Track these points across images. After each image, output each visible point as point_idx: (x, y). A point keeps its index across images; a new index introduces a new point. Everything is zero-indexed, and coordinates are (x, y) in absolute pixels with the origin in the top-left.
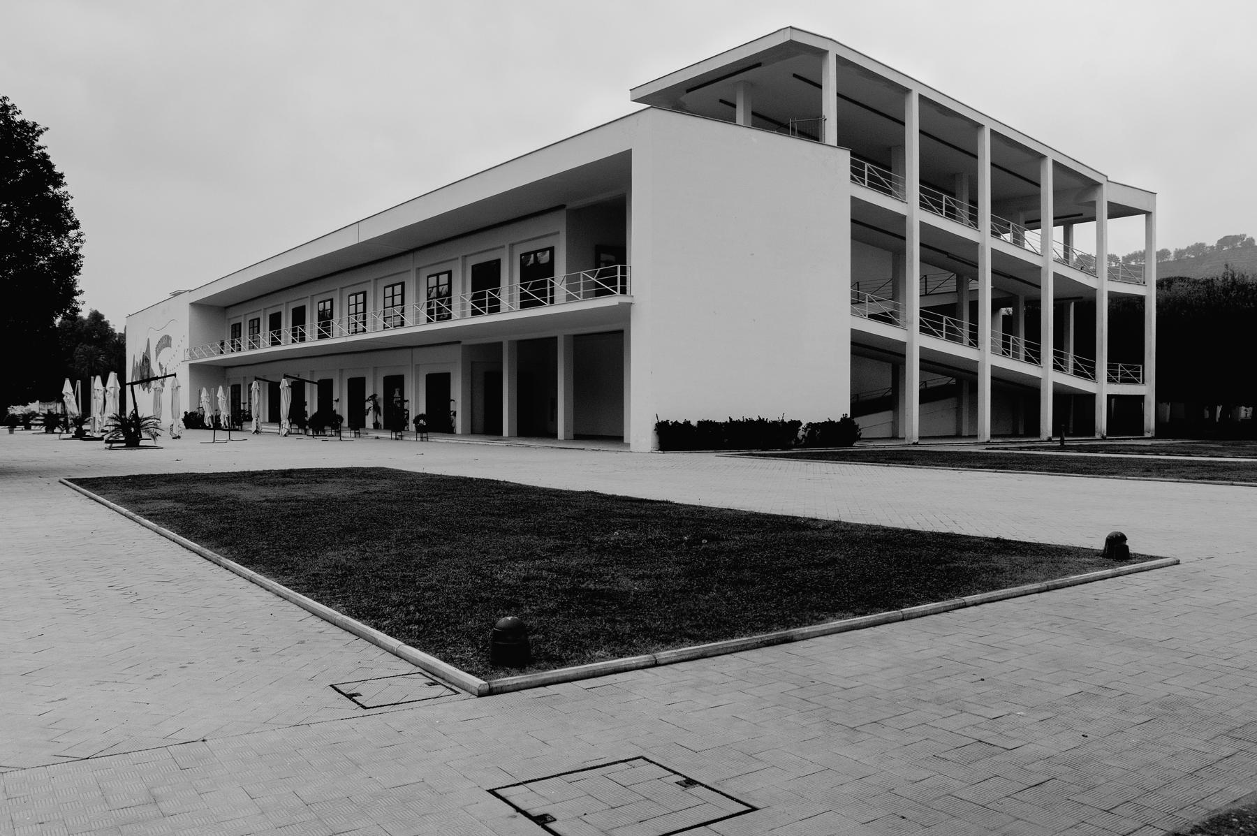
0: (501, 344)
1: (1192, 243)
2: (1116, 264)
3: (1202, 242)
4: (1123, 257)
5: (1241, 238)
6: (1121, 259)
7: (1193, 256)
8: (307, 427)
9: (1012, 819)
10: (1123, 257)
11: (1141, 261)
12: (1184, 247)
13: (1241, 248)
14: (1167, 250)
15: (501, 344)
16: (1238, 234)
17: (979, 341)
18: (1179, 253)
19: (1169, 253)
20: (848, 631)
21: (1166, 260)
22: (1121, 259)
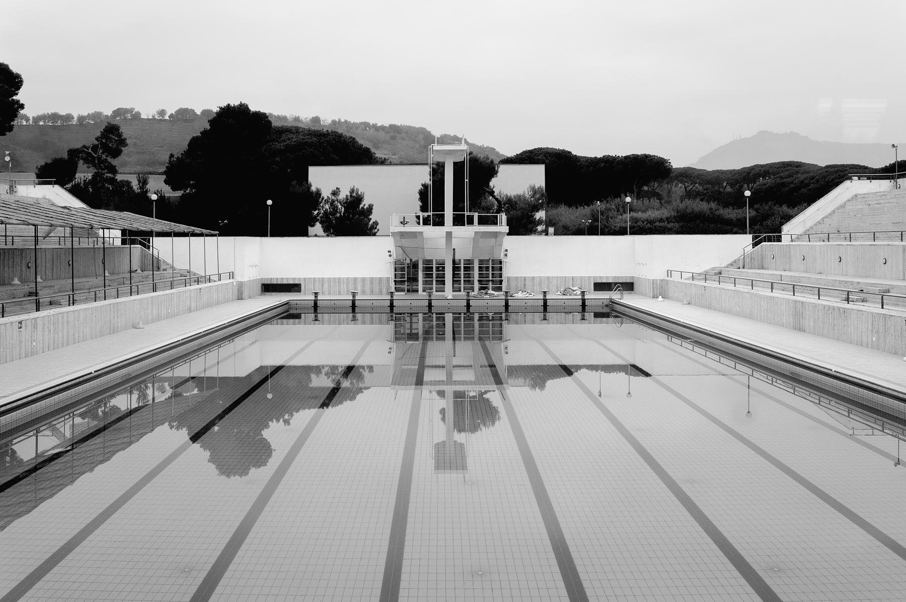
0: (479, 223)
1: (91, 111)
2: (27, 122)
3: (101, 111)
4: (33, 117)
5: (130, 111)
6: (31, 118)
7: (92, 122)
8: (167, 201)
9: (123, 549)
10: (33, 117)
11: (48, 122)
12: (85, 114)
13: (131, 119)
14: (71, 115)
15: (479, 223)
16: (128, 107)
17: (613, 281)
18: (81, 119)
19: (73, 118)
20: (154, 368)
21: (70, 123)
22: (31, 118)
